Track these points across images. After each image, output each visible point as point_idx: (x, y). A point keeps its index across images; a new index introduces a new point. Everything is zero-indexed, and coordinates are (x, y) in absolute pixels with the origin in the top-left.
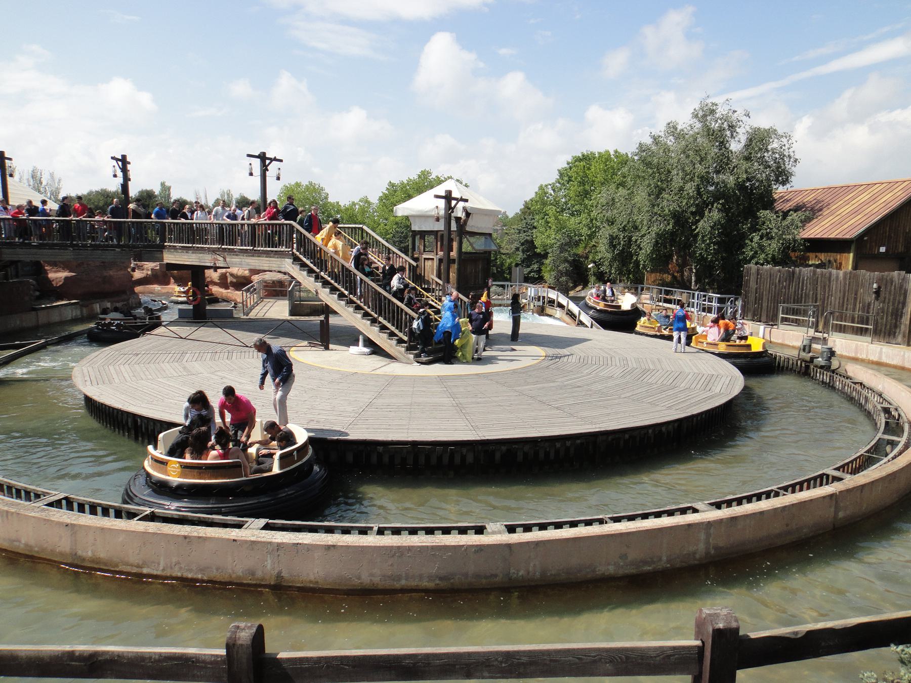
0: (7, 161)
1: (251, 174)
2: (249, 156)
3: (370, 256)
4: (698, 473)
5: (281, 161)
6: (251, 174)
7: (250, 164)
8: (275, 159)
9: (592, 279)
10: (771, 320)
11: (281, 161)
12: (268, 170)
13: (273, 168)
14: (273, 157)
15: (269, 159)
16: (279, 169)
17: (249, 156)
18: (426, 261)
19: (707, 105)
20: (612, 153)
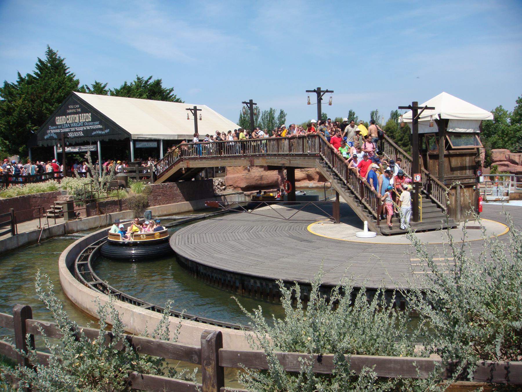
0: (254, 105)
1: (188, 119)
2: (307, 91)
3: (71, 135)
4: (170, 217)
5: (332, 92)
6: (188, 119)
7: (309, 97)
8: (327, 91)
9: (413, 356)
10: (10, 347)
11: (332, 92)
12: (322, 99)
13: (325, 98)
14: (325, 90)
15: (323, 91)
16: (331, 97)
17: (307, 91)
18: (137, 143)
19: (512, 144)
20: (517, 105)
